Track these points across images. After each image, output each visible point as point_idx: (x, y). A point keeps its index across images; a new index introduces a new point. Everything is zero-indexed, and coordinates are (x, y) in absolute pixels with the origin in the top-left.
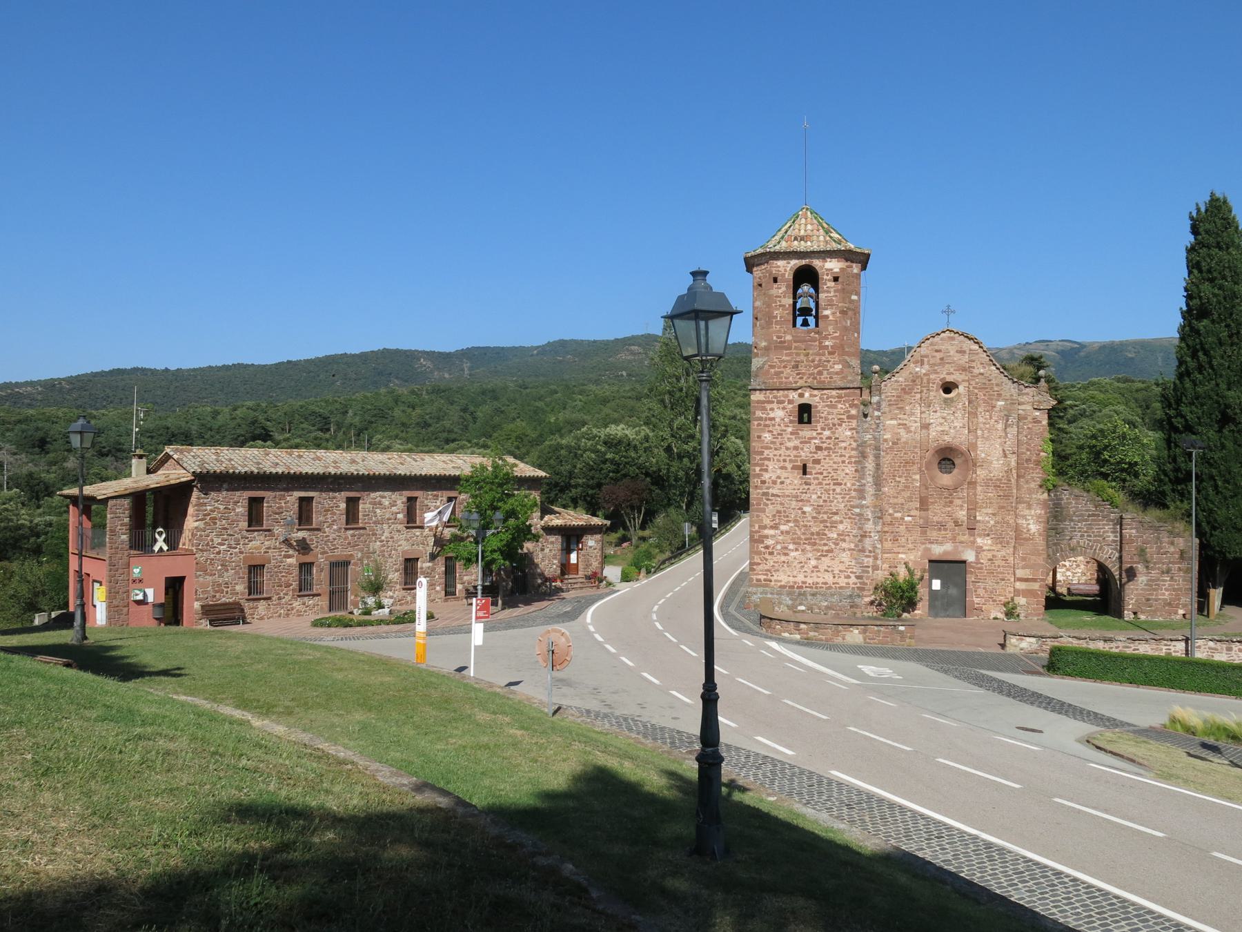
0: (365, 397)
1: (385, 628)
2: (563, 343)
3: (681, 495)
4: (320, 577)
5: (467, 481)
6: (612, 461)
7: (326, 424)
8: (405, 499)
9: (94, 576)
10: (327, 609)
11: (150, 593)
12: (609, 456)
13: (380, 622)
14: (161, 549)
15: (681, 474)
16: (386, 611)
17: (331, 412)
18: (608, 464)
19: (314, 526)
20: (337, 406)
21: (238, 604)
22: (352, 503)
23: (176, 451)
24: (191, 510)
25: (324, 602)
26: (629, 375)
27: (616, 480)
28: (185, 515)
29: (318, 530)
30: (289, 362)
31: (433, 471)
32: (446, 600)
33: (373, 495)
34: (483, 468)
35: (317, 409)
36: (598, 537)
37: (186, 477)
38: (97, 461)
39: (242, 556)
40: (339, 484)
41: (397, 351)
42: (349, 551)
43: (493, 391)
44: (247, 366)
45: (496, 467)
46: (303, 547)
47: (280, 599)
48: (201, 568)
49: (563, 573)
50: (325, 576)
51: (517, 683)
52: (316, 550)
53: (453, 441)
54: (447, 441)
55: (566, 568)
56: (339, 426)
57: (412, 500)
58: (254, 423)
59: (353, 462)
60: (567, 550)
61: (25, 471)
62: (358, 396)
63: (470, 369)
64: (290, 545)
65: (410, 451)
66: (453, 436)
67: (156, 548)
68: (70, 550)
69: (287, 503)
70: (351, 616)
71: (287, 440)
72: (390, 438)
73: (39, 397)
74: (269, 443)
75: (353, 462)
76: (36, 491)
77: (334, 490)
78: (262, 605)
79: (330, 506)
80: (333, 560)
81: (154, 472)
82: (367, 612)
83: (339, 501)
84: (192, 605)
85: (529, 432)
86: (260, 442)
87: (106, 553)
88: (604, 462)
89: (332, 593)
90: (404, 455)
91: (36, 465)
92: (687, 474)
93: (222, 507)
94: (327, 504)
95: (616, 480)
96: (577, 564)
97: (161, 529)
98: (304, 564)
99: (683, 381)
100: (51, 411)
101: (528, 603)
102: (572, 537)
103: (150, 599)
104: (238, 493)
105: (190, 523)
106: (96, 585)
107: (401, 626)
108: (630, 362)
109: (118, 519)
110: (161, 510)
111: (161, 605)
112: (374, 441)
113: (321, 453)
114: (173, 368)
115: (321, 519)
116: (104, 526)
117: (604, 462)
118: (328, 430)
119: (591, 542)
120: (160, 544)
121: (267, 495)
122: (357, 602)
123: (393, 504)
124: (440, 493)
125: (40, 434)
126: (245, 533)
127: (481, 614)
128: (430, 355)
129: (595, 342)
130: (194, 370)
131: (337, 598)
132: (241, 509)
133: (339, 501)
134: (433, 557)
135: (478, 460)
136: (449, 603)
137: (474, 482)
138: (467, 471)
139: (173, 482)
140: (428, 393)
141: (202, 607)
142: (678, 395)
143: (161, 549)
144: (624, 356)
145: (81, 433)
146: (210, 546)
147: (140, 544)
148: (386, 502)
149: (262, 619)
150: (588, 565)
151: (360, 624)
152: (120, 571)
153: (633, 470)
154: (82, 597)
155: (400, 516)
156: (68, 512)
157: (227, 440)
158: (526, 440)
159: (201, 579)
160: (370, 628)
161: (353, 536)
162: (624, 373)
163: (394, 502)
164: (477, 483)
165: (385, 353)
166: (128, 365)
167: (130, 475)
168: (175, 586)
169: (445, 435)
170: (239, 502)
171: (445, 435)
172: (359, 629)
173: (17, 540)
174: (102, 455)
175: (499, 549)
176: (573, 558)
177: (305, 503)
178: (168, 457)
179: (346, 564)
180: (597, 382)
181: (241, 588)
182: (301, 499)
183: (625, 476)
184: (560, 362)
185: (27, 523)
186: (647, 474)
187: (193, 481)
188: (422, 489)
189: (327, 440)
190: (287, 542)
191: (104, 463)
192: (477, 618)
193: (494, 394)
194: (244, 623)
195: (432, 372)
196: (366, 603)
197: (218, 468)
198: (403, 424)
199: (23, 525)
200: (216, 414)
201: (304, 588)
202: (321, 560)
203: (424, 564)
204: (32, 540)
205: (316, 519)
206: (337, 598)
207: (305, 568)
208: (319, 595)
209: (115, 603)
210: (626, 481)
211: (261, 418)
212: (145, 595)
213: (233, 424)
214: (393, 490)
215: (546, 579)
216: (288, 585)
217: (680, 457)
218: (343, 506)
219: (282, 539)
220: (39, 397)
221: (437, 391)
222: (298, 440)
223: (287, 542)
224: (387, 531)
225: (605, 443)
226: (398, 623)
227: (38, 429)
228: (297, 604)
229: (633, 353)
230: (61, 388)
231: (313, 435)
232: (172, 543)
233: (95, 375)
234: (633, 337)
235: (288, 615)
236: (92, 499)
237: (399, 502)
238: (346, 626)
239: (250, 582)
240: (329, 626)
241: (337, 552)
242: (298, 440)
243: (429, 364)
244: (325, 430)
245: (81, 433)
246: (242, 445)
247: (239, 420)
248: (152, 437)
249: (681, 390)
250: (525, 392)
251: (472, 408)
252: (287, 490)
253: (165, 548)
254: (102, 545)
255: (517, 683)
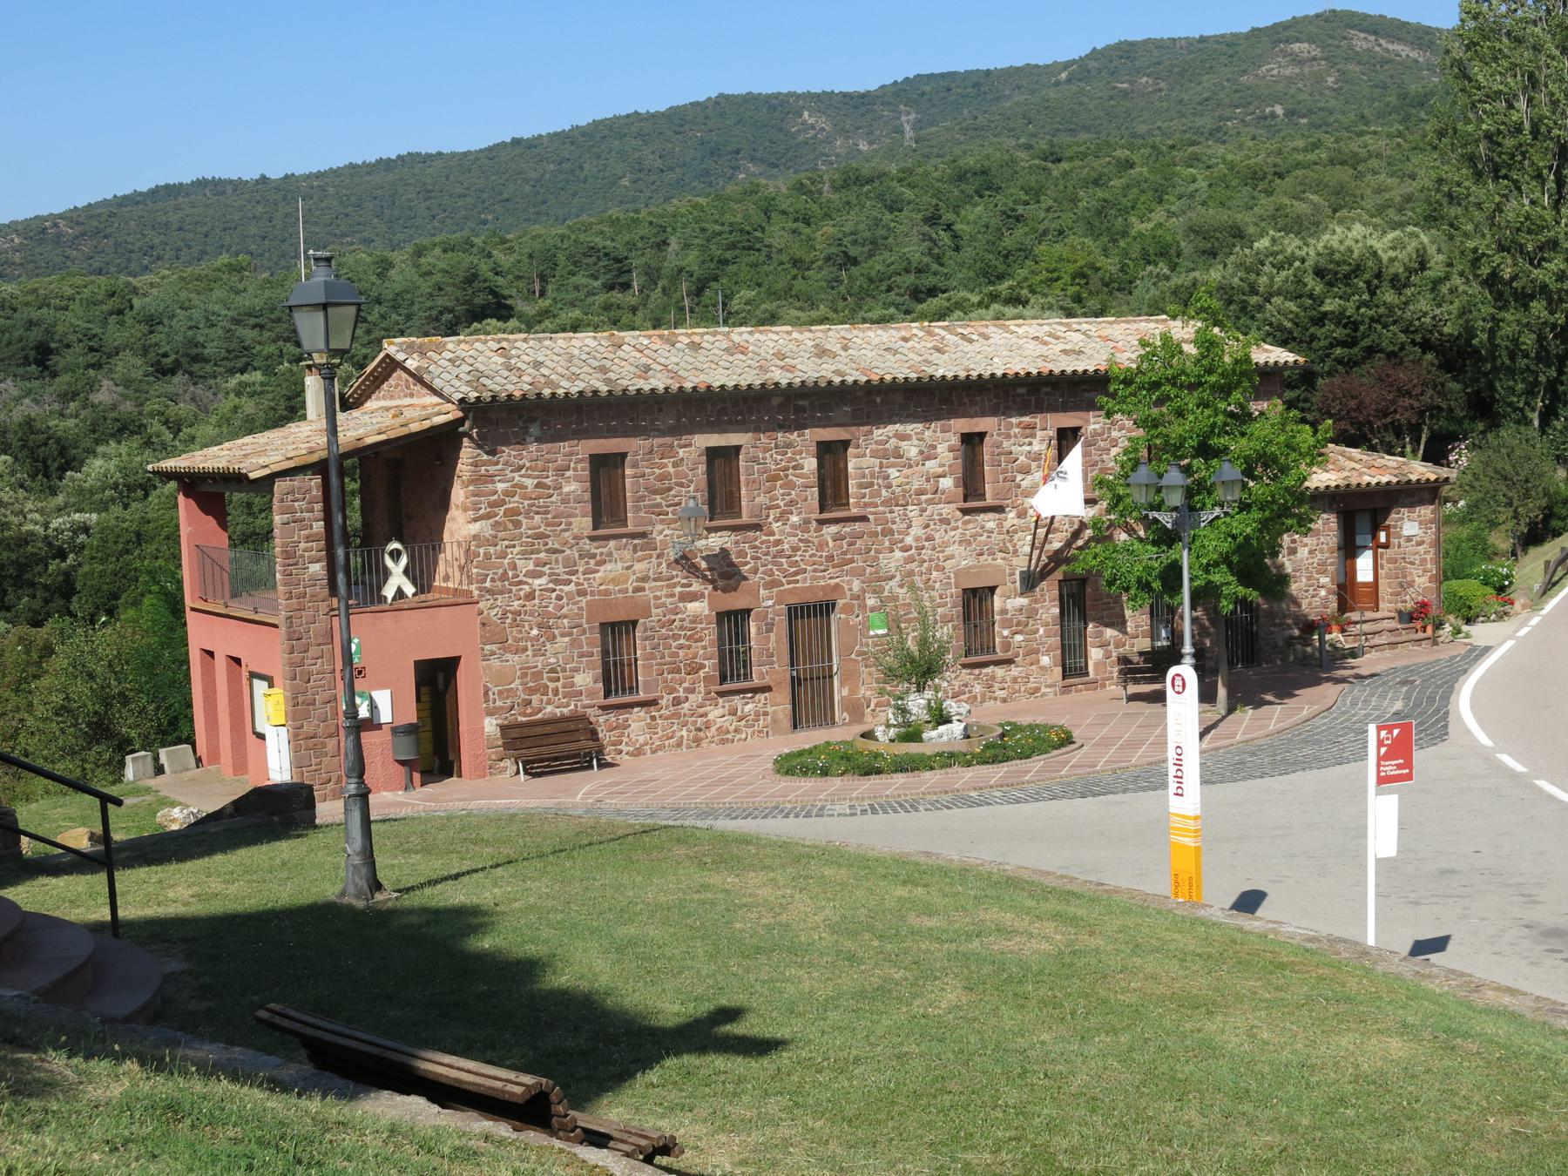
0: (696, 206)
1: (963, 776)
2: (1126, 52)
3: (1530, 392)
4: (767, 643)
5: (1127, 382)
6: (1339, 318)
7: (621, 272)
8: (955, 440)
9: (251, 663)
10: (787, 723)
11: (383, 698)
12: (1330, 305)
13: (949, 759)
14: (400, 593)
15: (1529, 340)
16: (956, 728)
17: (631, 245)
18: (1329, 326)
19: (745, 518)
20: (645, 230)
21: (584, 718)
22: (832, 455)
23: (410, 349)
24: (458, 494)
25: (778, 705)
26: (1290, 113)
27: (1350, 364)
28: (444, 504)
29: (757, 527)
30: (516, 142)
31: (1000, 366)
32: (1066, 689)
33: (879, 433)
34: (1171, 347)
35: (599, 241)
36: (1426, 511)
37: (446, 414)
38: (159, 387)
39: (584, 601)
40: (799, 410)
41: (750, 100)
42: (830, 578)
43: (984, 172)
44: (429, 156)
45: (1208, 346)
46: (725, 572)
47: (677, 702)
48: (495, 635)
49: (1343, 607)
50: (777, 641)
51: (1439, 944)
52: (755, 579)
53: (932, 292)
54: (918, 295)
55: (1348, 593)
56: (652, 275)
57: (972, 441)
58: (472, 278)
59: (821, 352)
60: (1349, 550)
61: (18, 414)
62: (680, 204)
63: (918, 125)
64: (693, 570)
65: (822, 321)
66: (928, 281)
67: (389, 592)
68: (188, 603)
69: (670, 467)
70: (872, 746)
71: (545, 314)
72: (773, 294)
73: (17, 258)
74: (513, 323)
75: (821, 352)
76: (47, 461)
77: (786, 427)
78: (637, 720)
79: (781, 463)
80: (794, 600)
81: (357, 404)
82: (912, 735)
83: (799, 453)
84: (479, 726)
85: (1102, 261)
86: (493, 322)
87: (279, 606)
88: (1320, 320)
89: (796, 682)
90: (938, 327)
91: (37, 402)
92: (1541, 338)
93: (530, 483)
94: (773, 460)
95: (1350, 364)
96: (1375, 583)
97: (395, 545)
98: (728, 613)
99: (1522, 104)
100: (48, 284)
101: (1285, 691)
102: (1362, 513)
103: (385, 716)
104: (565, 447)
105: (459, 526)
106: (260, 686)
107: (1003, 769)
108: (1290, 80)
109: (297, 521)
110: (394, 493)
111: (411, 730)
112: (735, 305)
113: (741, 334)
114: (275, 174)
115: (762, 499)
116: (268, 535)
117: (1320, 320)
118: (626, 286)
119: (1410, 525)
120: (397, 580)
121: (634, 446)
122: (867, 708)
123: (928, 455)
124: (1038, 419)
125: (35, 335)
126: (587, 545)
127: (1390, 768)
128: (823, 101)
129: (1203, 39)
130: (319, 175)
131: (809, 697)
132: (575, 486)
133: (799, 453)
134: (1030, 582)
135: (1152, 327)
136: (1074, 697)
137: (1152, 385)
138: (1128, 358)
139: (415, 427)
140: (835, 189)
141: (504, 729)
142: (1509, 143)
143: (400, 593)
144: (1275, 69)
145: (325, 307)
146: (509, 580)
147: (355, 583)
148: (911, 450)
149: (638, 752)
150: (1405, 586)
151: (904, 766)
152: (313, 651)
153: (1390, 337)
154: (361, 775)
155: (947, 483)
156: (176, 506)
157: (416, 322)
158: (1095, 279)
159: (495, 663)
160: (929, 778)
161: (838, 538)
162: (1279, 110)
163: (928, 449)
164: (1155, 385)
165: (723, 105)
166: (184, 175)
167: (304, 417)
168: (436, 680)
169: (910, 279)
170: (563, 469)
171: (910, 279)
172: (900, 778)
173: (22, 568)
174: (164, 371)
175: (1226, 559)
176: (1364, 567)
177: (721, 461)
178: (391, 365)
179: (825, 609)
180: (1217, 134)
181: (587, 679)
182: (713, 454)
183: (1370, 351)
184: (1125, 94)
185: (39, 529)
186: (1426, 346)
187: (460, 422)
188: (994, 411)
189: (634, 310)
190: (685, 561)
191: (170, 389)
192: (1381, 780)
193: (984, 182)
194: (602, 765)
195: (829, 141)
196: (904, 711)
197: (516, 386)
198: (796, 262)
199: (31, 533)
200: (385, 266)
201: (733, 668)
202: (766, 606)
203: (1007, 602)
204: (53, 566)
205: (750, 501)
206: (809, 697)
207: (733, 622)
208: (766, 689)
209: (308, 728)
210: (1379, 360)
211: (484, 268)
212: (373, 707)
213: (425, 286)
214: (926, 418)
215: (1309, 627)
216: (694, 669)
217: (1524, 299)
218: (810, 464)
219: (672, 554)
220: (17, 258)
221: (851, 180)
222: (576, 313)
223: (685, 561)
224: (918, 528)
225: (1319, 273)
226: (995, 760)
227: (31, 324)
228: (716, 713)
229: (1297, 60)
230: (59, 236)
231: (601, 298)
232: (421, 575)
233: (122, 202)
234: (1295, 22)
235: (698, 741)
236: (236, 479)
237: (942, 448)
238: (869, 771)
239: (605, 665)
240: (825, 773)
241: (804, 582)
242: (576, 313)
243: (823, 123)
244: (621, 283)
245: (325, 307)
246: (451, 331)
247: (438, 277)
248: (262, 327)
249: (1518, 129)
250: (1057, 170)
251: (949, 216)
252: (676, 431)
253: (409, 589)
254: (267, 583)
255: (1439, 944)
